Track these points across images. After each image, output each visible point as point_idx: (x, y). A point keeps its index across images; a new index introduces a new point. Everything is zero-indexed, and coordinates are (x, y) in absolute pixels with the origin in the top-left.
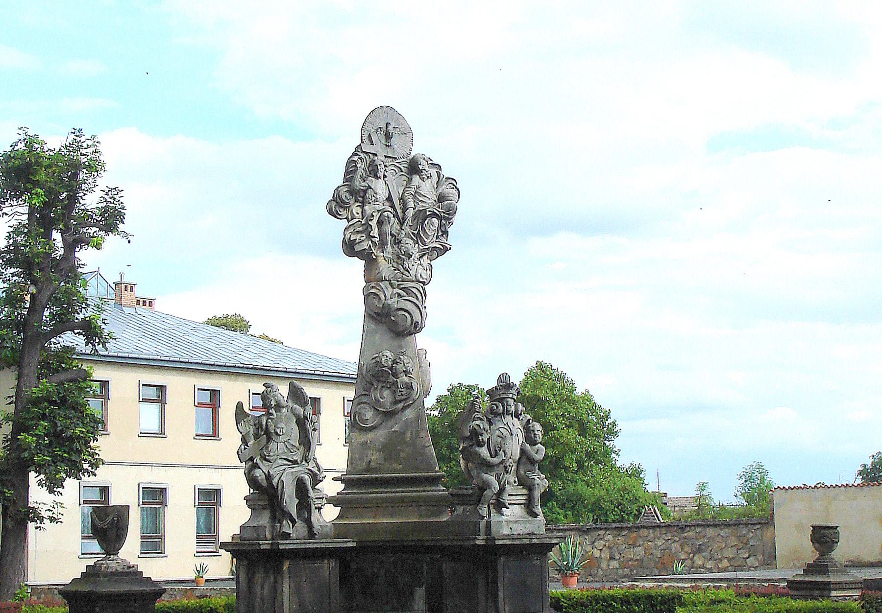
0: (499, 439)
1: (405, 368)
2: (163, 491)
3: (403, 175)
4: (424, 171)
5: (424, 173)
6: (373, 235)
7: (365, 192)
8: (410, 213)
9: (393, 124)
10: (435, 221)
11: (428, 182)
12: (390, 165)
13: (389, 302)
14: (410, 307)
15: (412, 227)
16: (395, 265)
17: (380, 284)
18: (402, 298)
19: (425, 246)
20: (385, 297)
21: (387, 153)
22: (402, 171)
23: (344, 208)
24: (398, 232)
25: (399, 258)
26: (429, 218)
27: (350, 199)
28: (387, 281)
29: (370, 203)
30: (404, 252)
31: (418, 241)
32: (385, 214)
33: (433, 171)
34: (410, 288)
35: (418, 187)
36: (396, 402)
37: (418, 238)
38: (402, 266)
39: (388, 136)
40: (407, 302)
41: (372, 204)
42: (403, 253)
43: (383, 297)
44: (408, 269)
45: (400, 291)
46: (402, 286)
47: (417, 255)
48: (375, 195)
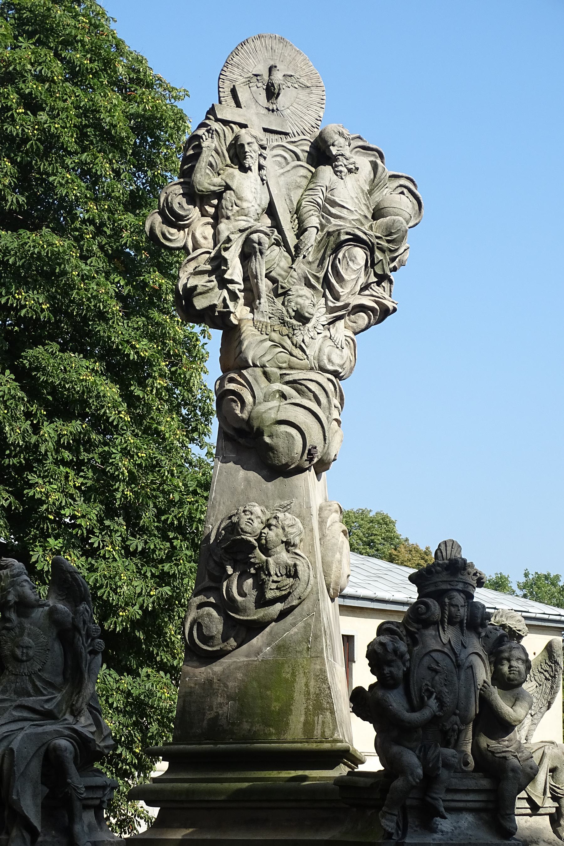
1: (286, 536)
5: (342, 161)
7: (219, 196)
11: (350, 179)
12: (274, 147)
13: (262, 408)
16: (275, 336)
20: (254, 397)
22: (299, 159)
23: (180, 228)
29: (228, 218)
32: (255, 237)
38: (289, 338)
41: (232, 218)
42: (293, 314)
43: (248, 398)
44: (303, 345)
46: (287, 378)
47: (325, 319)
48: (237, 201)
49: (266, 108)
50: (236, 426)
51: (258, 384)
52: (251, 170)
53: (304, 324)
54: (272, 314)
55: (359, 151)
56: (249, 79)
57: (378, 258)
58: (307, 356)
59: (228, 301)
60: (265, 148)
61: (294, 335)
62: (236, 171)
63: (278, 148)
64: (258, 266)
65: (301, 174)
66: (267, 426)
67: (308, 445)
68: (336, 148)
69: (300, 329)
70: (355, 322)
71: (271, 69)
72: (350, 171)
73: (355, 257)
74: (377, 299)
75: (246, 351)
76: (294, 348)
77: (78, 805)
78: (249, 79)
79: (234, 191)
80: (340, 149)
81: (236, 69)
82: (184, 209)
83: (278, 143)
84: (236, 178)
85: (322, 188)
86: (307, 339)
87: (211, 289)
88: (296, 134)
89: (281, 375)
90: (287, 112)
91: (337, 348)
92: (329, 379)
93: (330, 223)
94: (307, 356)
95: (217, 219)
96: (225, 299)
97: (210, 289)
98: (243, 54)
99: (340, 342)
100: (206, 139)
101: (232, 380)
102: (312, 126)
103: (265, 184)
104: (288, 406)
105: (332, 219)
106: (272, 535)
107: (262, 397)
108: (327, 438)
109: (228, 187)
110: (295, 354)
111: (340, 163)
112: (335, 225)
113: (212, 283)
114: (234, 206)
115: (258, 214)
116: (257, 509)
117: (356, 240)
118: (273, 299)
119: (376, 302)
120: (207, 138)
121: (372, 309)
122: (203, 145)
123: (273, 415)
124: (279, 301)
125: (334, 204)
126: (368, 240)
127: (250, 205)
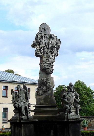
0: (70, 97)
2: (7, 109)
7: (40, 42)
8: (50, 47)
9: (46, 27)
10: (55, 49)
13: (45, 67)
14: (50, 68)
16: (47, 58)
23: (35, 46)
25: (47, 57)
33: (55, 38)
35: (52, 41)
36: (47, 89)
37: (52, 53)
39: (45, 30)
47: (52, 56)
62: (42, 39)
71: (45, 27)
77: (28, 112)
90: (47, 32)
95: (39, 45)
101: (42, 64)
106: (48, 81)
109: (41, 41)
116: (45, 78)
117: (55, 47)
123: (47, 68)
124: (47, 54)
125: (52, 43)
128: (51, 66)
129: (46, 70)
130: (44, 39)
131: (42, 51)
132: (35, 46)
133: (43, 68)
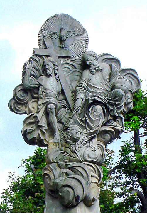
3: (76, 71)
4: (92, 66)
5: (93, 67)
6: (40, 125)
7: (38, 88)
8: (79, 103)
10: (99, 108)
11: (98, 76)
12: (64, 64)
13: (57, 180)
14: (73, 183)
15: (81, 115)
16: (63, 148)
17: (50, 166)
18: (69, 176)
19: (92, 130)
21: (61, 53)
22: (75, 68)
23: (23, 105)
24: (66, 120)
25: (67, 142)
26: (93, 106)
27: (24, 96)
28: (55, 162)
29: (42, 98)
30: (70, 137)
31: (86, 126)
32: (49, 106)
34: (75, 167)
35: (89, 80)
37: (85, 124)
38: (70, 149)
39: (62, 40)
40: (72, 179)
41: (43, 98)
42: (70, 138)
43: (52, 177)
44: (76, 151)
45: (68, 170)
46: (69, 166)
47: (86, 139)
48: (44, 91)
49: (60, 47)
50: (50, 189)
51: (56, 170)
52: (52, 76)
53: (75, 142)
54: (62, 138)
55: (106, 61)
56: (51, 35)
57: (110, 109)
58: (78, 155)
59: (41, 135)
60: (56, 66)
61: (71, 147)
62: (44, 78)
63: (65, 64)
64: (52, 119)
65: (77, 75)
66: (60, 188)
67: (75, 195)
68: (89, 61)
69: (73, 144)
70: (104, 138)
71: (61, 29)
72: (97, 71)
73: (96, 110)
74: (113, 127)
75: (49, 156)
76: (71, 153)
78: (51, 35)
79: (43, 86)
80: (91, 62)
81: (45, 32)
82: (22, 96)
83: (66, 62)
84: (44, 80)
85: (85, 80)
86: (77, 148)
87: (34, 130)
88: (75, 57)
89: (66, 165)
91: (93, 151)
92: (88, 165)
93: (89, 95)
94: (78, 155)
96: (39, 134)
97: (33, 130)
98: (48, 24)
99: (94, 148)
100: (28, 65)
102: (82, 52)
103: (59, 81)
104: (69, 178)
105: (90, 93)
107: (58, 176)
108: (84, 191)
109: (40, 85)
110: (71, 155)
111: (92, 68)
112: (91, 96)
113: (34, 128)
114: (43, 93)
115: (55, 95)
117: (97, 103)
118: (62, 132)
119: (112, 128)
120: (29, 64)
121: (111, 131)
122: (27, 68)
123: (63, 183)
126: (102, 102)
127: (50, 91)
128: (82, 176)
129: (60, 194)
130: (56, 74)
131: (43, 123)
132: (20, 104)
133: (51, 184)
